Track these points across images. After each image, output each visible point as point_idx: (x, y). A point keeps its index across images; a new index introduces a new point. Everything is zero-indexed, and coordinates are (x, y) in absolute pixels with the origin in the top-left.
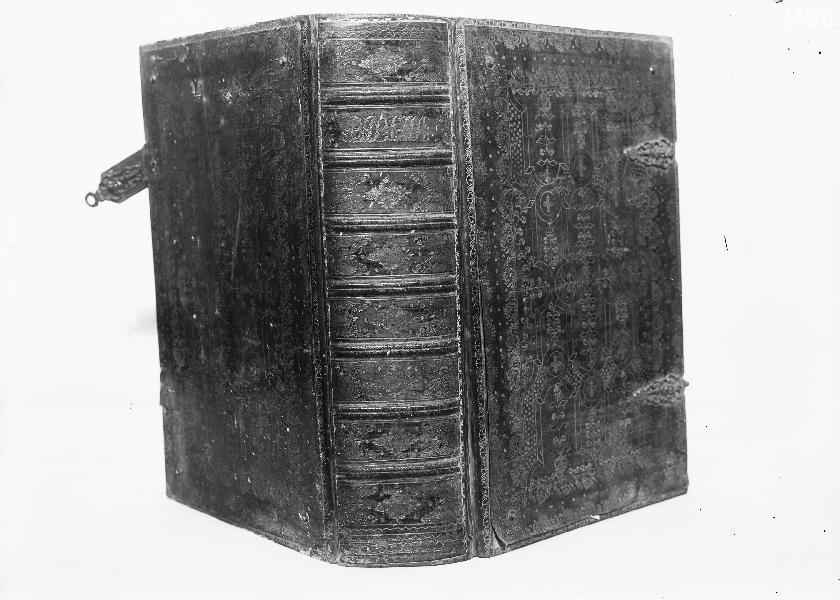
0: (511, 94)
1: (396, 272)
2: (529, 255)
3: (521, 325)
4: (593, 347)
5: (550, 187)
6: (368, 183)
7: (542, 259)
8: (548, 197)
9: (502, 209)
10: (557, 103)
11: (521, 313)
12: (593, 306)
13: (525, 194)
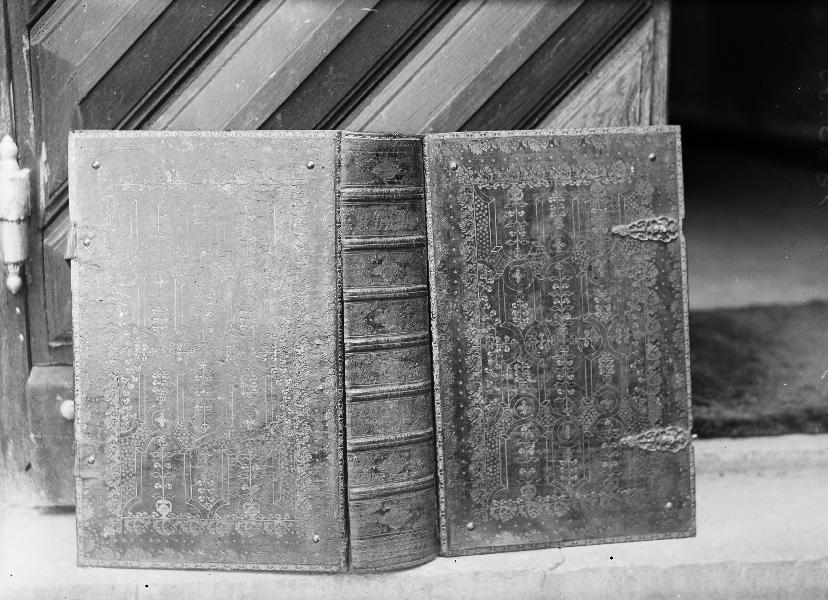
0: (477, 189)
1: (392, 331)
2: (494, 317)
3: (484, 374)
4: (570, 396)
5: (521, 262)
6: (374, 262)
7: (511, 321)
8: (518, 270)
9: (464, 281)
10: (529, 193)
11: (485, 363)
12: (572, 362)
13: (491, 267)
